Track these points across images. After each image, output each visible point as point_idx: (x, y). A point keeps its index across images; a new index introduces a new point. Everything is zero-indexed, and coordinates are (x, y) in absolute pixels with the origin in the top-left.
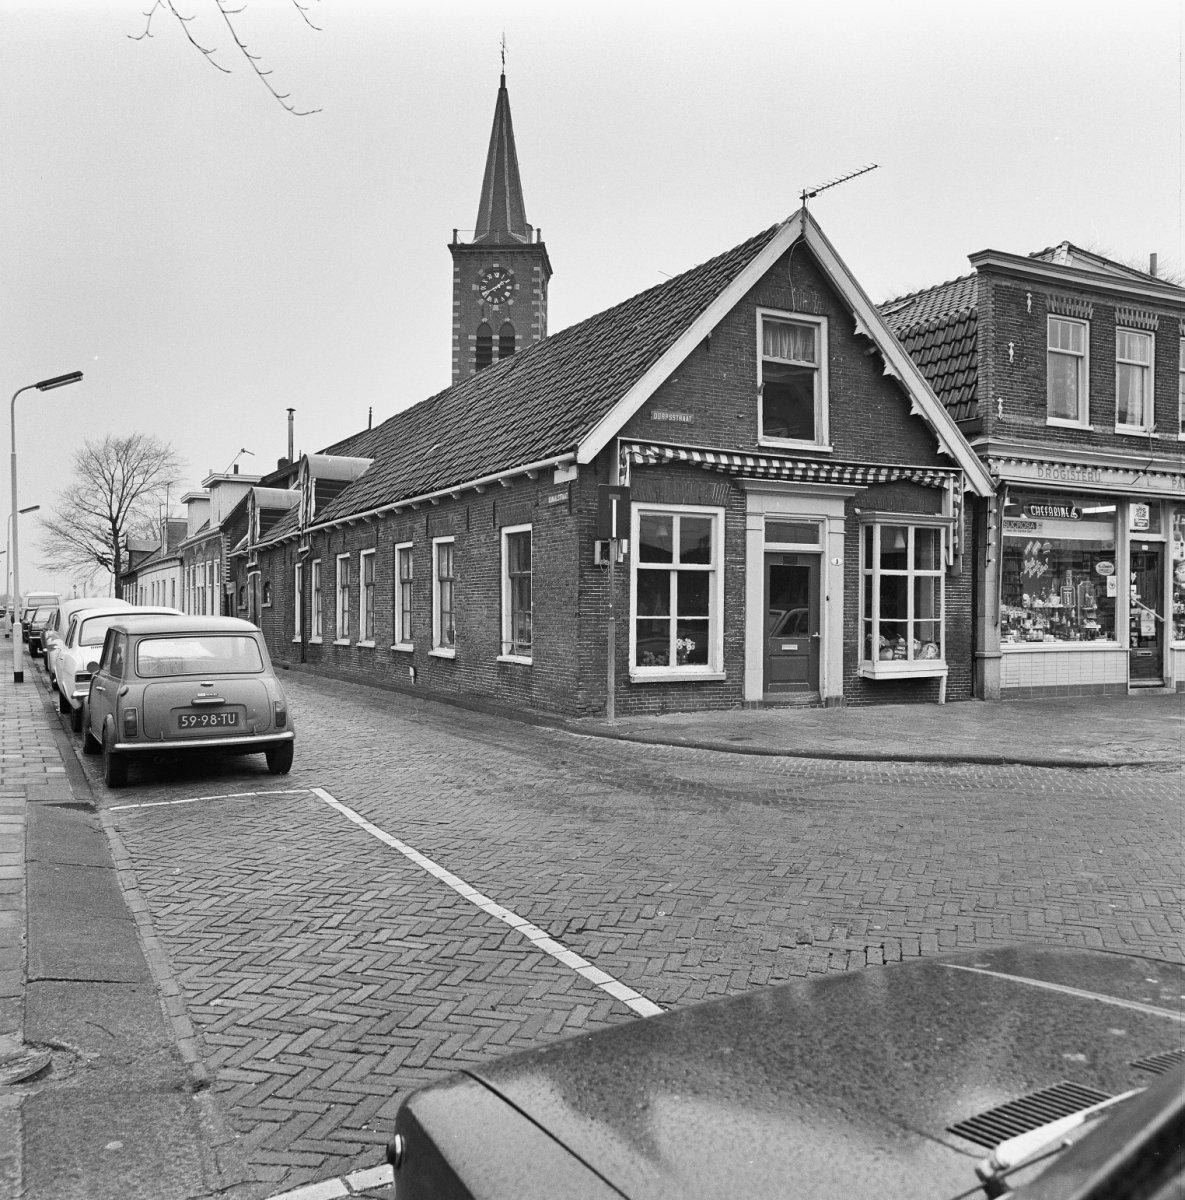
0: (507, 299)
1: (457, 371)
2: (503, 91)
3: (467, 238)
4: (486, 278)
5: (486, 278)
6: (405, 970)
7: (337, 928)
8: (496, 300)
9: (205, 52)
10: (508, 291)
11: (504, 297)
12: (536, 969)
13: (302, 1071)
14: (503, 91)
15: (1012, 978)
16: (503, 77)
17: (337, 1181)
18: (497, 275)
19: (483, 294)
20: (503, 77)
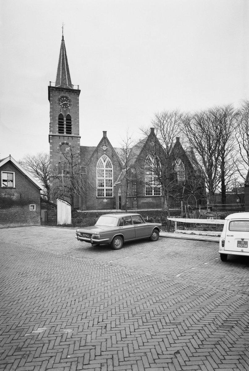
0: (68, 107)
1: (52, 151)
2: (63, 47)
3: (53, 85)
4: (61, 99)
5: (61, 99)
6: (12, 314)
7: (39, 296)
8: (64, 107)
9: (174, 331)
10: (68, 104)
11: (67, 106)
12: (19, 338)
13: (21, 360)
14: (63, 47)
15: (91, 211)
16: (63, 37)
17: (51, 86)
18: (65, 99)
19: (61, 104)
20: (63, 37)
